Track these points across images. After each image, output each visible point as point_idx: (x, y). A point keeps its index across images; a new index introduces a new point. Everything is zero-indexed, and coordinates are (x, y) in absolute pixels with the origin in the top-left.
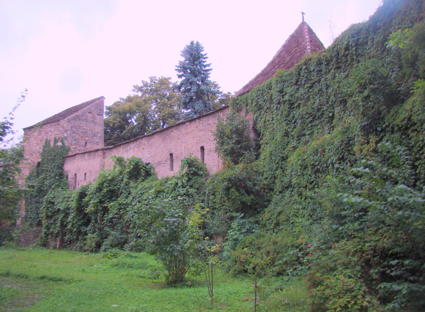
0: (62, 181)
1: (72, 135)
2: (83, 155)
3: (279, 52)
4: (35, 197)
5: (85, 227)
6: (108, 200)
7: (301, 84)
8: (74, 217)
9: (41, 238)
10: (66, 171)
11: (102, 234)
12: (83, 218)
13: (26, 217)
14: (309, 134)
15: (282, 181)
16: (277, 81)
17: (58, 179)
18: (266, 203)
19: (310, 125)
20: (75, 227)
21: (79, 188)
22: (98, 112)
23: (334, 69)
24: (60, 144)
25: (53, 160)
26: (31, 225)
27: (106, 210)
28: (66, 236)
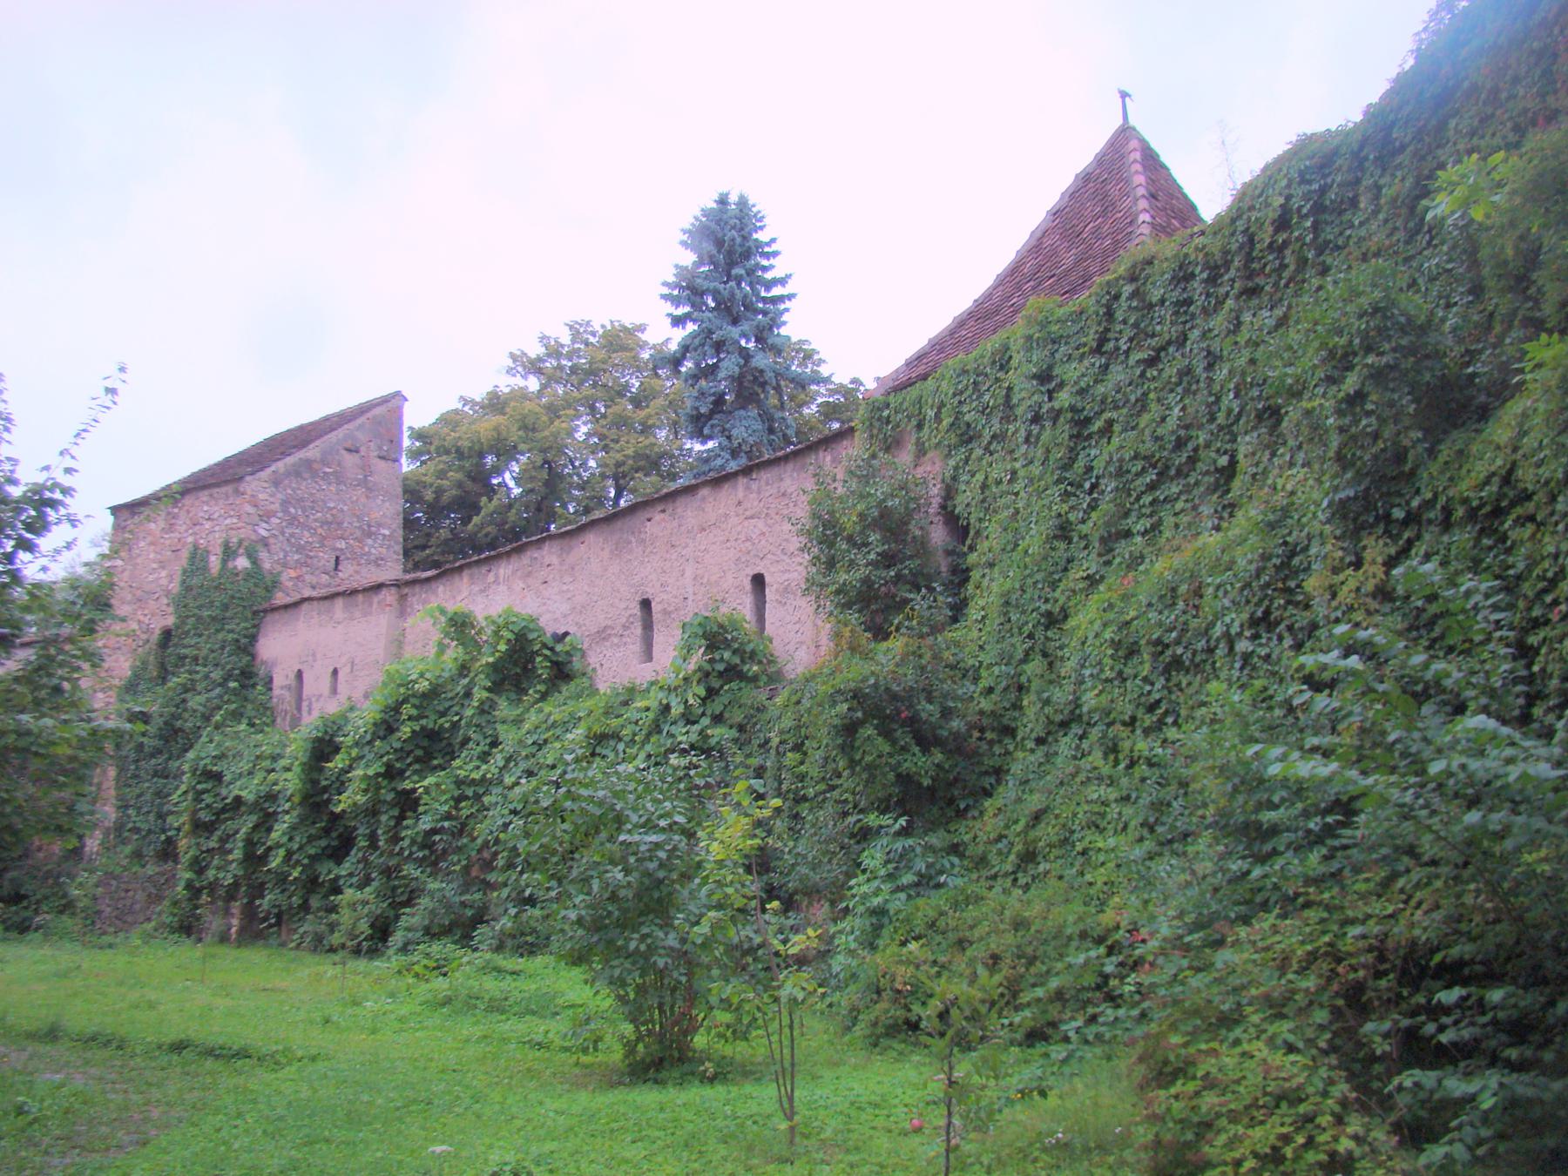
0: (251, 697)
2: (327, 603)
3: (1039, 234)
4: (152, 756)
5: (331, 864)
7: (1117, 348)
8: (293, 828)
9: (175, 903)
10: (263, 663)
11: (394, 888)
12: (327, 831)
13: (119, 827)
14: (1146, 532)
15: (1047, 702)
16: (1029, 338)
17: (235, 692)
18: (988, 781)
19: (1147, 499)
20: (298, 862)
22: (380, 448)
23: (1237, 298)
24: (242, 563)
25: (219, 621)
26: (138, 855)
27: (408, 803)
28: (262, 897)
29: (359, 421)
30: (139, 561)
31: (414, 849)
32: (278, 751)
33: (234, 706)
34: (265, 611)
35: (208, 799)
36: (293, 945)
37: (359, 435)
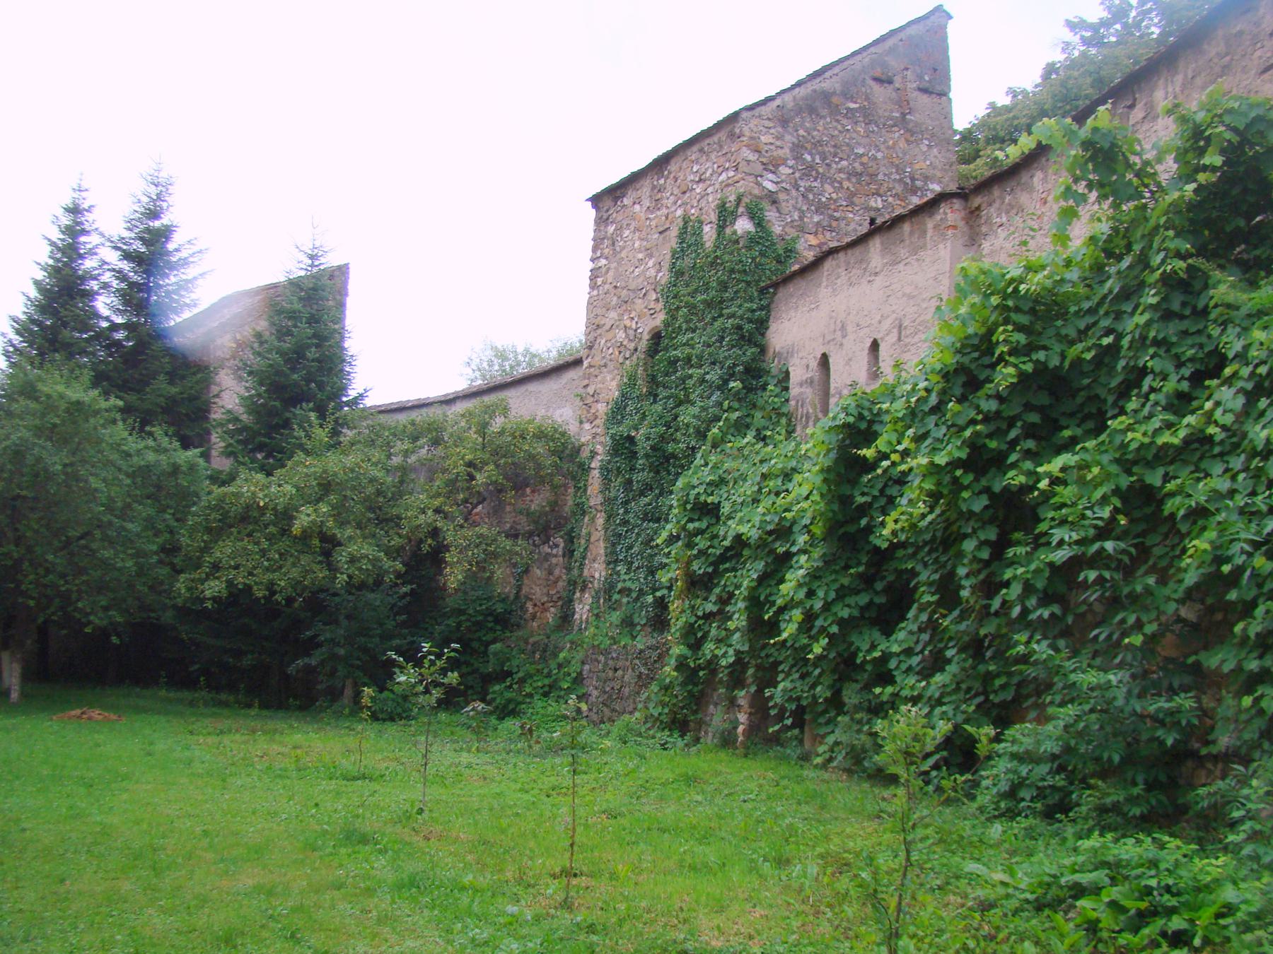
0: (760, 402)
1: (802, 183)
2: (857, 251)
4: (642, 494)
5: (876, 634)
6: (1030, 444)
8: (814, 575)
9: (666, 688)
10: (775, 355)
11: (988, 678)
12: (867, 581)
13: (609, 588)
17: (738, 397)
20: (823, 630)
21: (838, 413)
22: (920, 77)
24: (743, 225)
25: (715, 305)
26: (628, 623)
27: (1016, 515)
28: (774, 684)
30: (623, 254)
31: (1032, 602)
32: (793, 463)
33: (737, 414)
34: (776, 285)
35: (701, 542)
36: (818, 760)
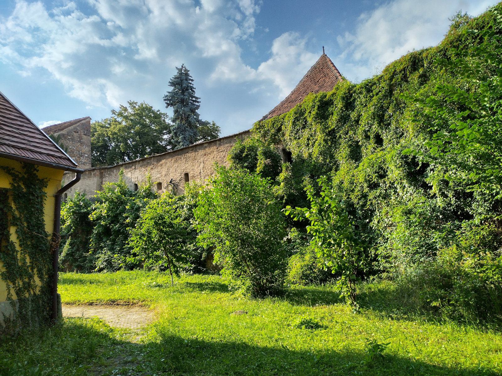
22: (84, 132)
29: (78, 124)
37: (78, 128)
